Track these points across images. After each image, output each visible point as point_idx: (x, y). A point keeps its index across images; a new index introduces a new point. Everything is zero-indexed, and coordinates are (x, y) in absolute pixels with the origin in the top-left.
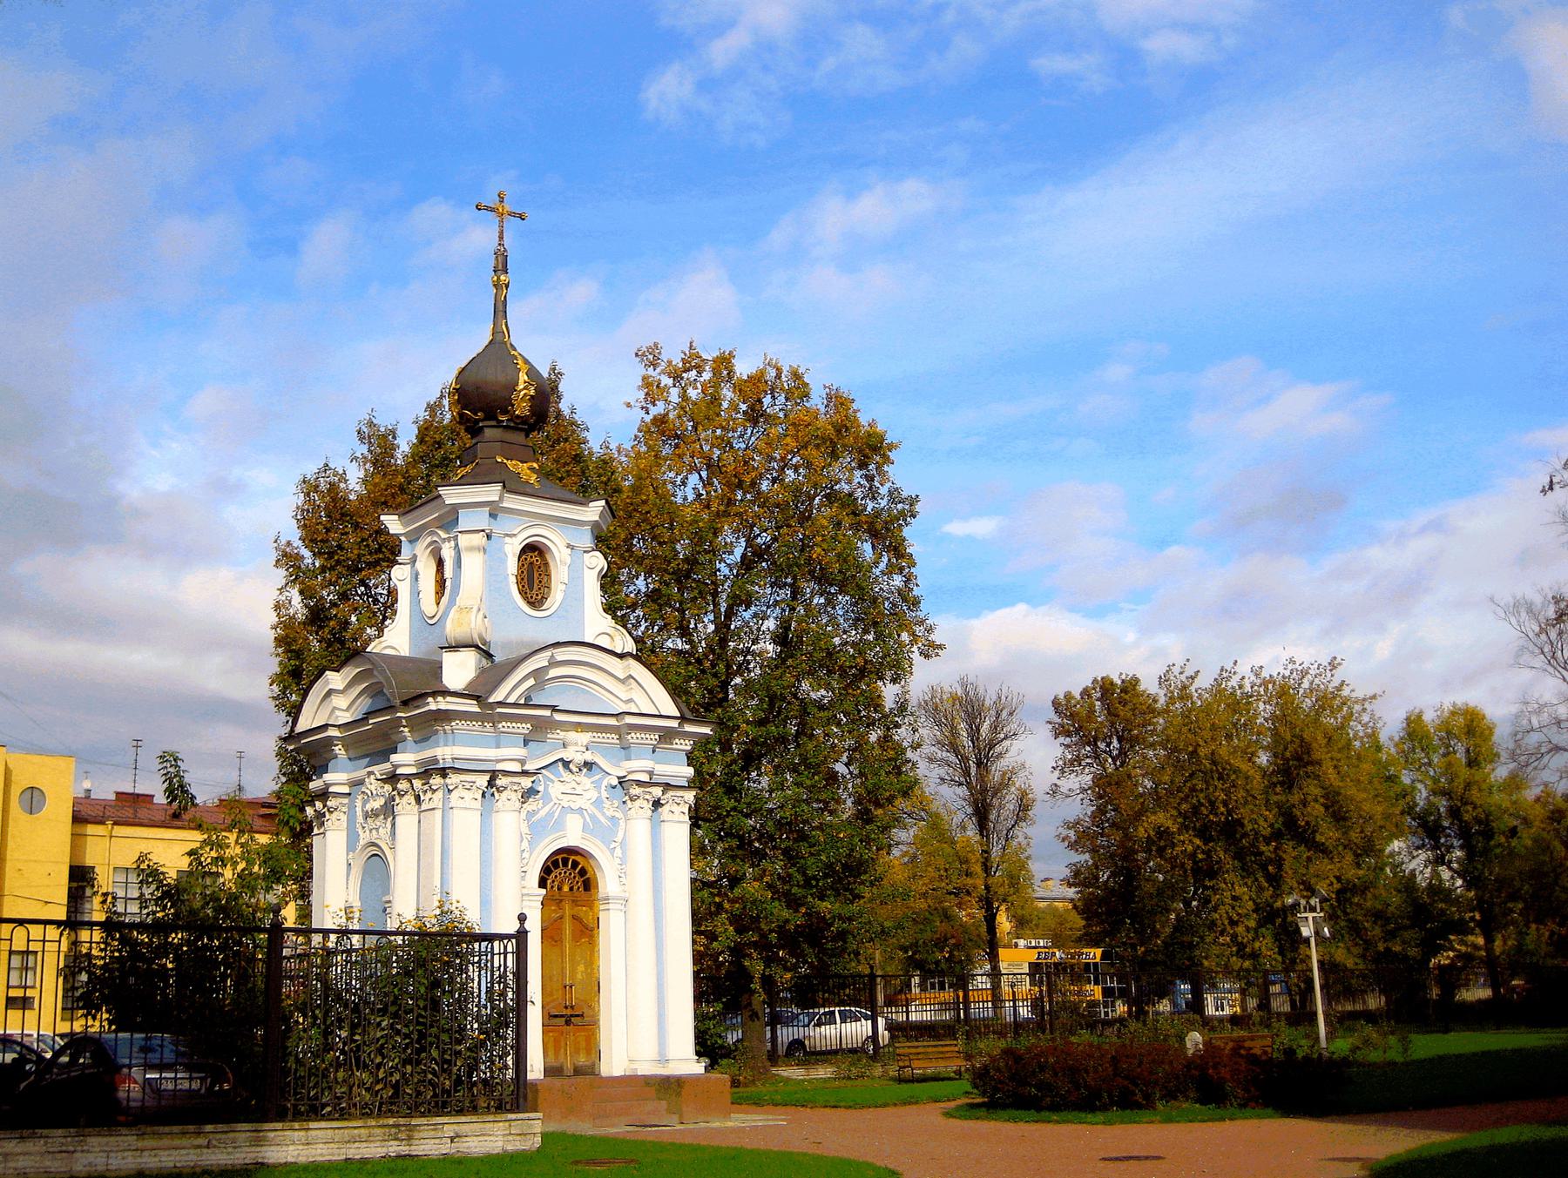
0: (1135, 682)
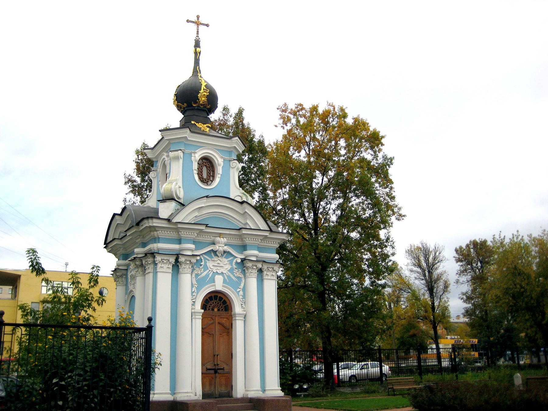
0: (485, 241)
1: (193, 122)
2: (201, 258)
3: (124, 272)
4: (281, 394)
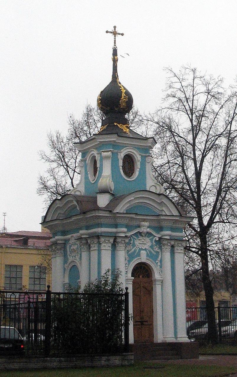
1: (115, 124)
2: (131, 238)
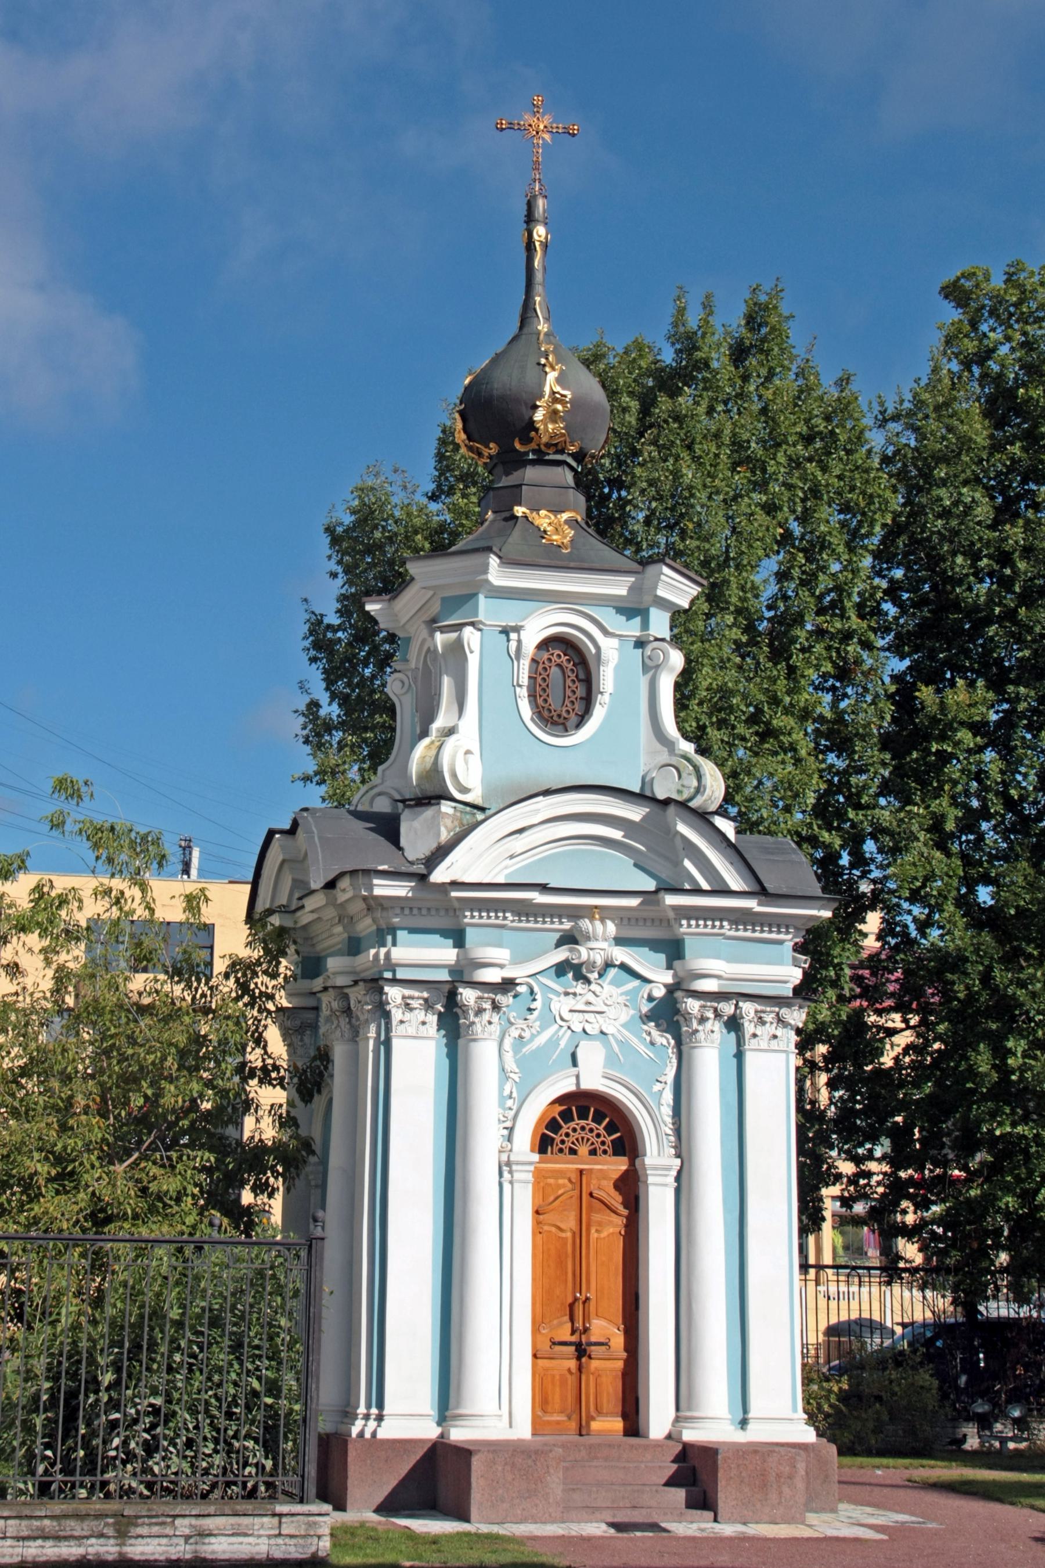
3: (310, 1016)
4: (808, 1435)
